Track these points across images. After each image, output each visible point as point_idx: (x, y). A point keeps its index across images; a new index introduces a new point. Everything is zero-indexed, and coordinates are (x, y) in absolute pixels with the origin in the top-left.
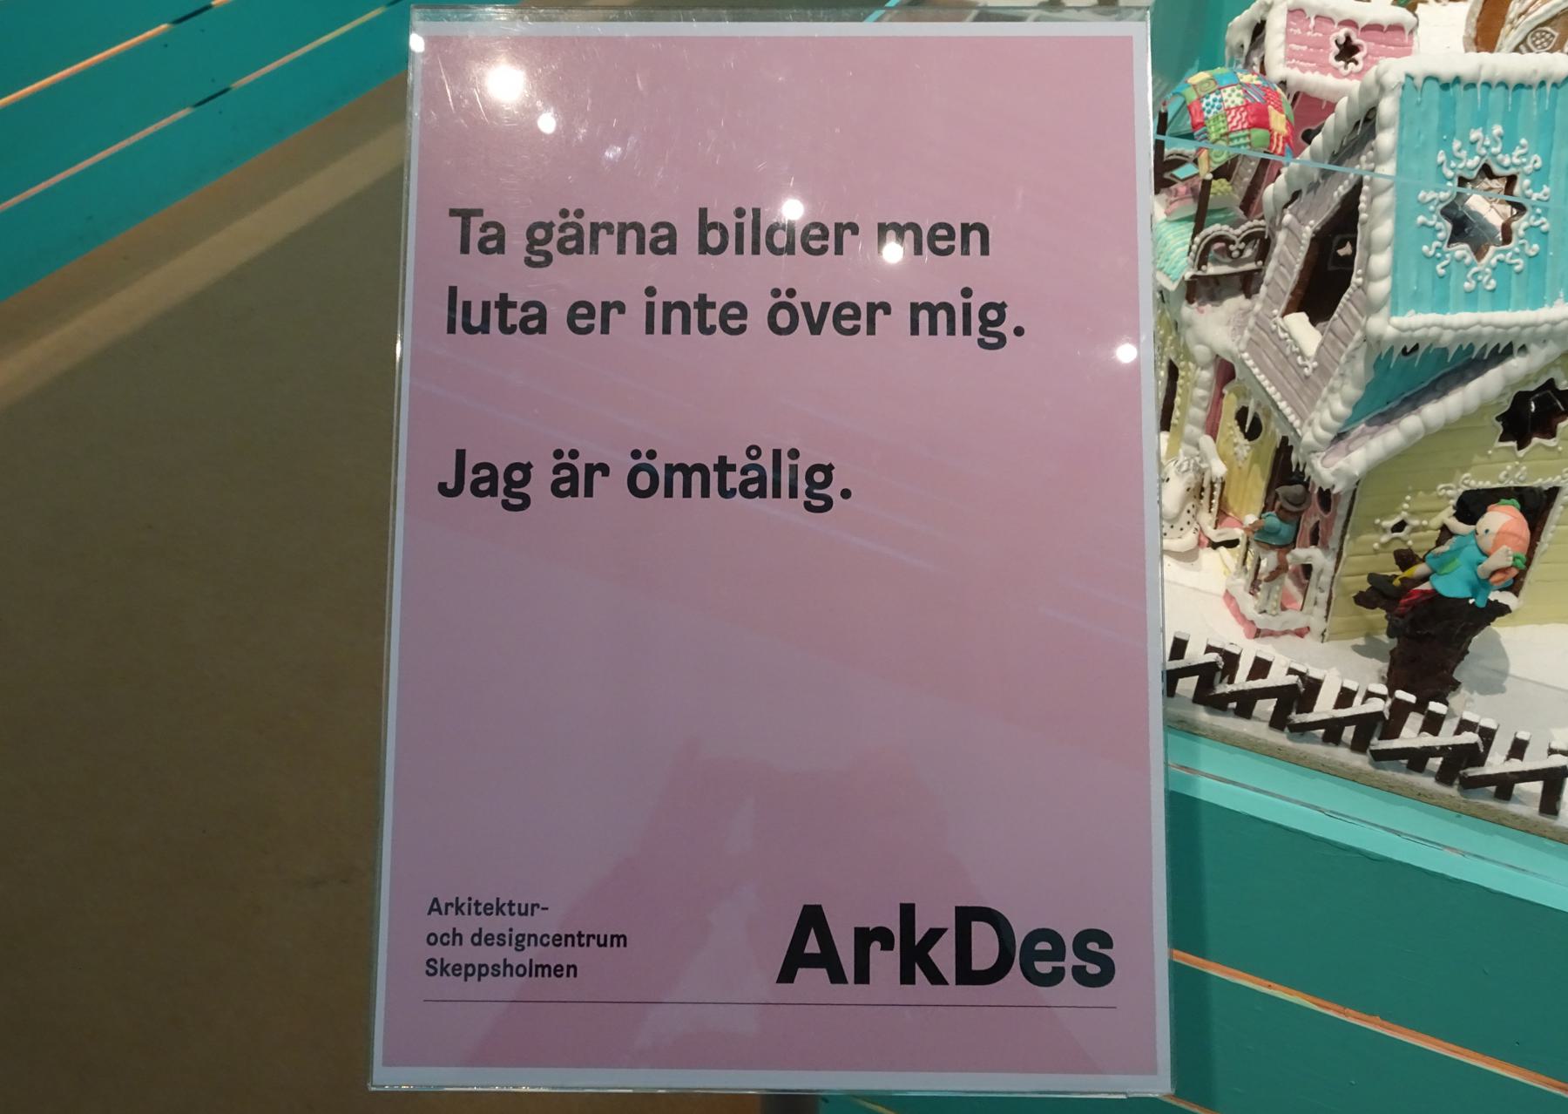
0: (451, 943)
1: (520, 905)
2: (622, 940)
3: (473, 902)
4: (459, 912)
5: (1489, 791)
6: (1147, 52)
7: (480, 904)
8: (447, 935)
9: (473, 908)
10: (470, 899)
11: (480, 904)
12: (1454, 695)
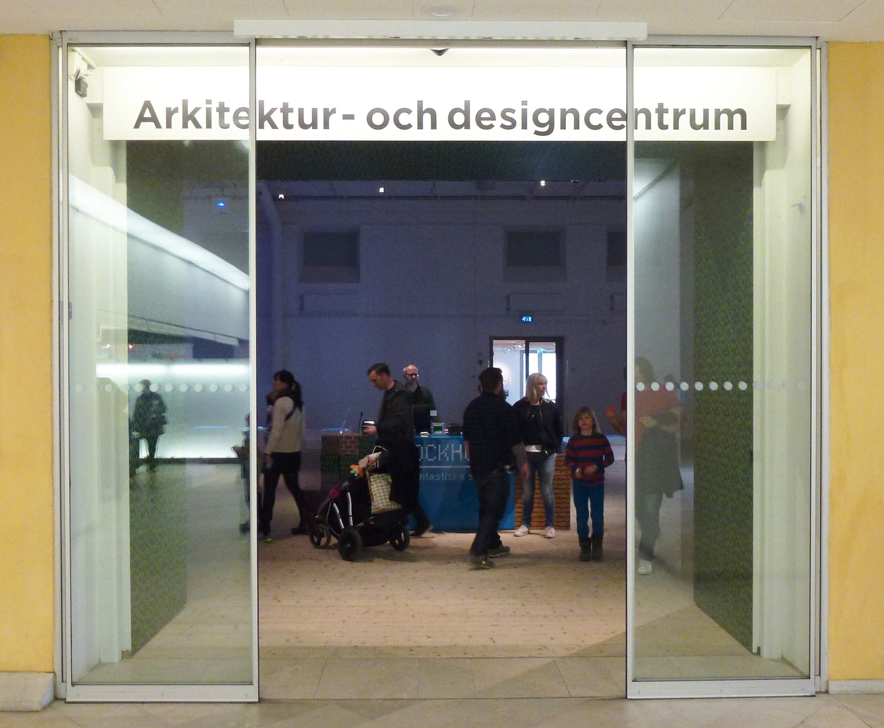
0: (415, 124)
1: (301, 112)
2: (737, 118)
3: (214, 106)
4: (190, 123)
5: (388, 544)
6: (831, 491)
7: (227, 110)
8: (409, 111)
9: (215, 116)
10: (209, 102)
11: (227, 110)
12: (244, 482)
